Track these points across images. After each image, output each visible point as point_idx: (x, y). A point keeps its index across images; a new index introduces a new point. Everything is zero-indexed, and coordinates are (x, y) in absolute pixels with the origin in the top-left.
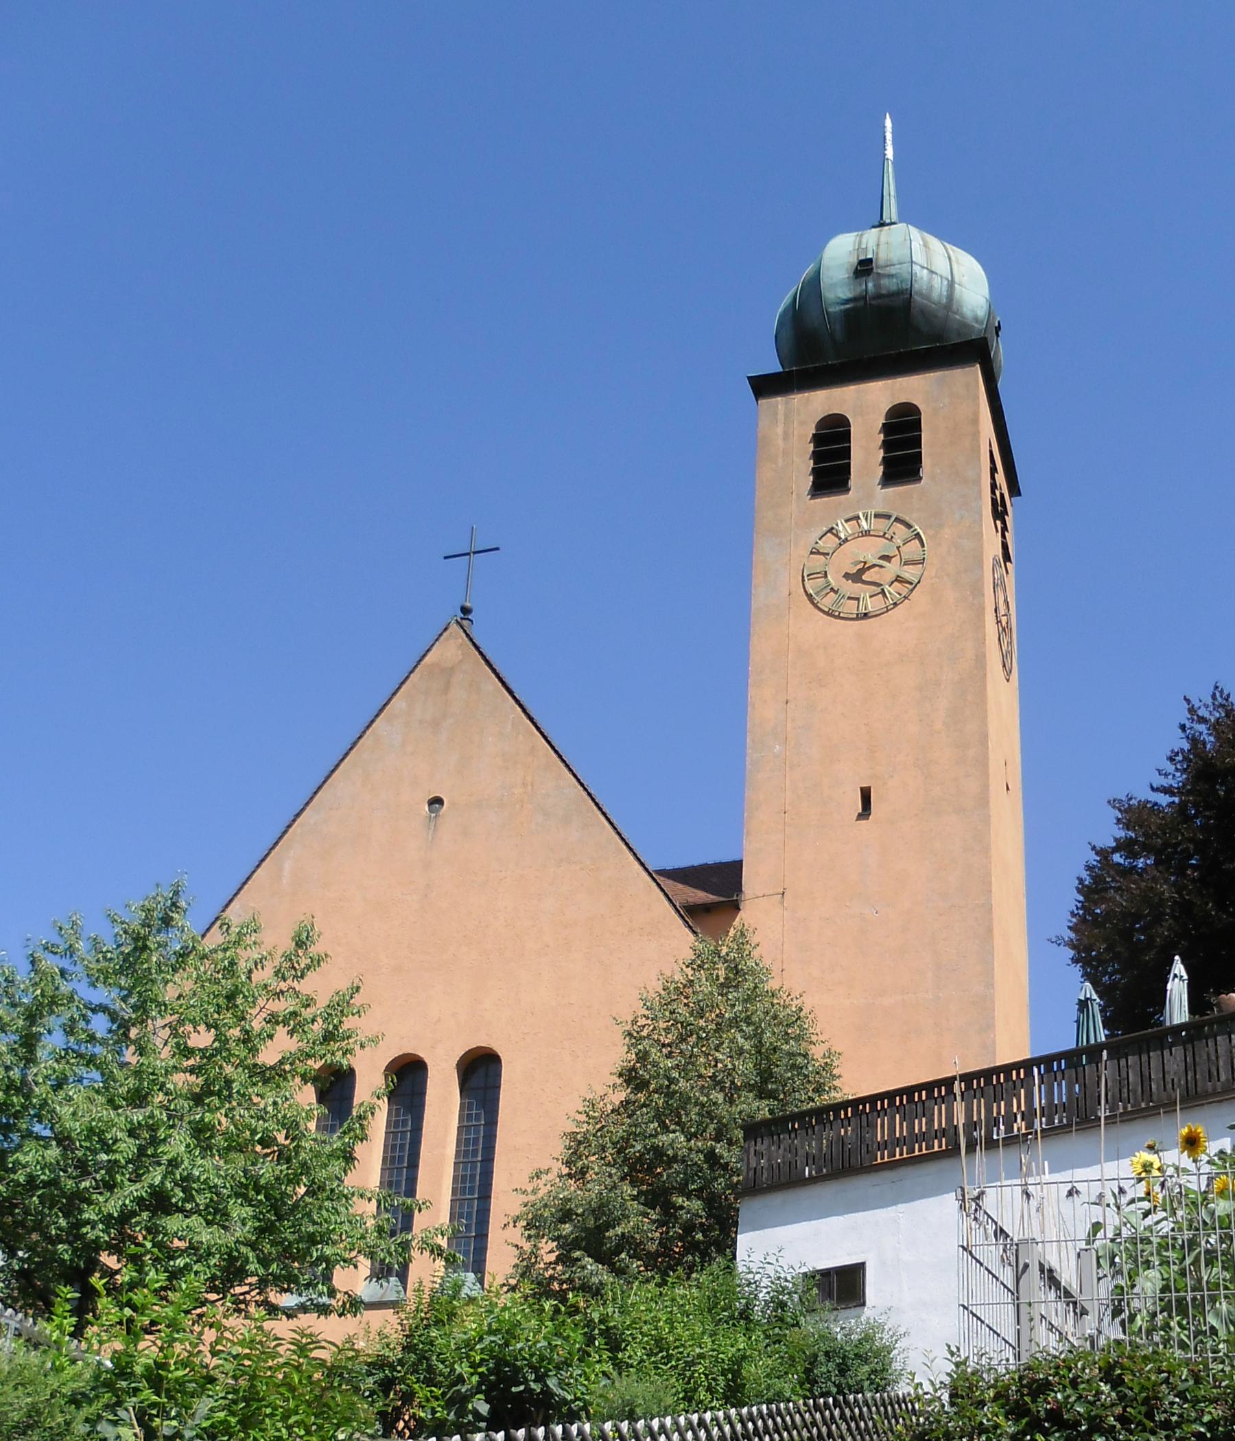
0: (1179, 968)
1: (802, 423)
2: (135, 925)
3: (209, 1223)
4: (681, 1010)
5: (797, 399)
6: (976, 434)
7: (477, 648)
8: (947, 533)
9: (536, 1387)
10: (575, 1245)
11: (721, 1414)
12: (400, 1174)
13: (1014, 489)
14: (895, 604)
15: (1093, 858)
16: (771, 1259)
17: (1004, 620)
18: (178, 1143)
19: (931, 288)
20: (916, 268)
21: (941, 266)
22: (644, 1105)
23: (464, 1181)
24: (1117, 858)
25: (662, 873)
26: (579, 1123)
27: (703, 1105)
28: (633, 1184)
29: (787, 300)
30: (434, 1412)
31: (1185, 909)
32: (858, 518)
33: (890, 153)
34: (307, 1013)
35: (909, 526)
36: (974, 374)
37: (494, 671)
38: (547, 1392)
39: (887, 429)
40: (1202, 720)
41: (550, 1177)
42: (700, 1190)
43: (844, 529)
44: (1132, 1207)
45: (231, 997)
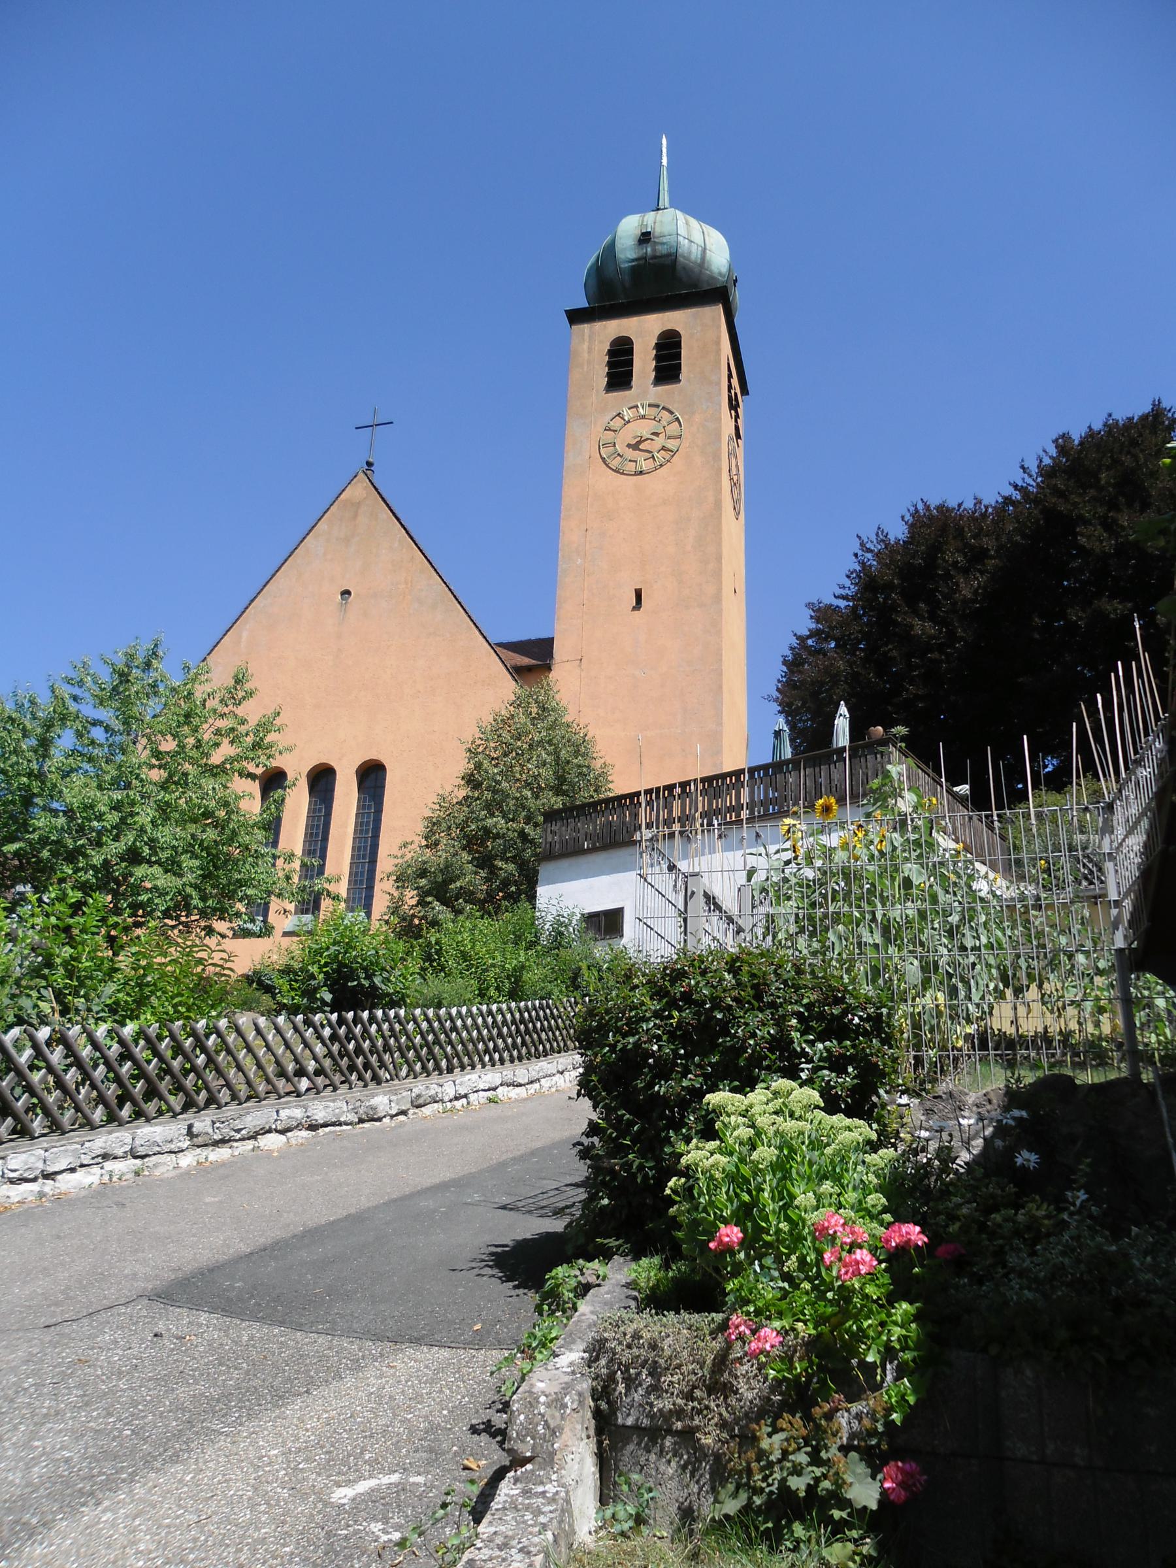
0: (843, 709)
1: (601, 342)
2: (121, 666)
3: (166, 871)
4: (505, 734)
5: (598, 326)
6: (718, 351)
7: (376, 489)
8: (697, 418)
9: (366, 983)
10: (428, 893)
11: (504, 1006)
12: (316, 845)
13: (745, 390)
14: (661, 466)
15: (795, 642)
16: (554, 902)
17: (735, 478)
18: (145, 815)
19: (690, 252)
20: (680, 239)
21: (697, 237)
22: (478, 799)
23: (359, 850)
24: (810, 642)
25: (499, 645)
26: (433, 810)
27: (517, 799)
28: (469, 853)
29: (593, 259)
30: (293, 999)
31: (855, 676)
32: (637, 407)
33: (665, 161)
34: (242, 729)
35: (671, 413)
36: (719, 309)
37: (387, 505)
38: (373, 987)
39: (658, 347)
40: (869, 550)
41: (413, 846)
42: (514, 857)
43: (628, 414)
44: (777, 856)
45: (187, 716)
